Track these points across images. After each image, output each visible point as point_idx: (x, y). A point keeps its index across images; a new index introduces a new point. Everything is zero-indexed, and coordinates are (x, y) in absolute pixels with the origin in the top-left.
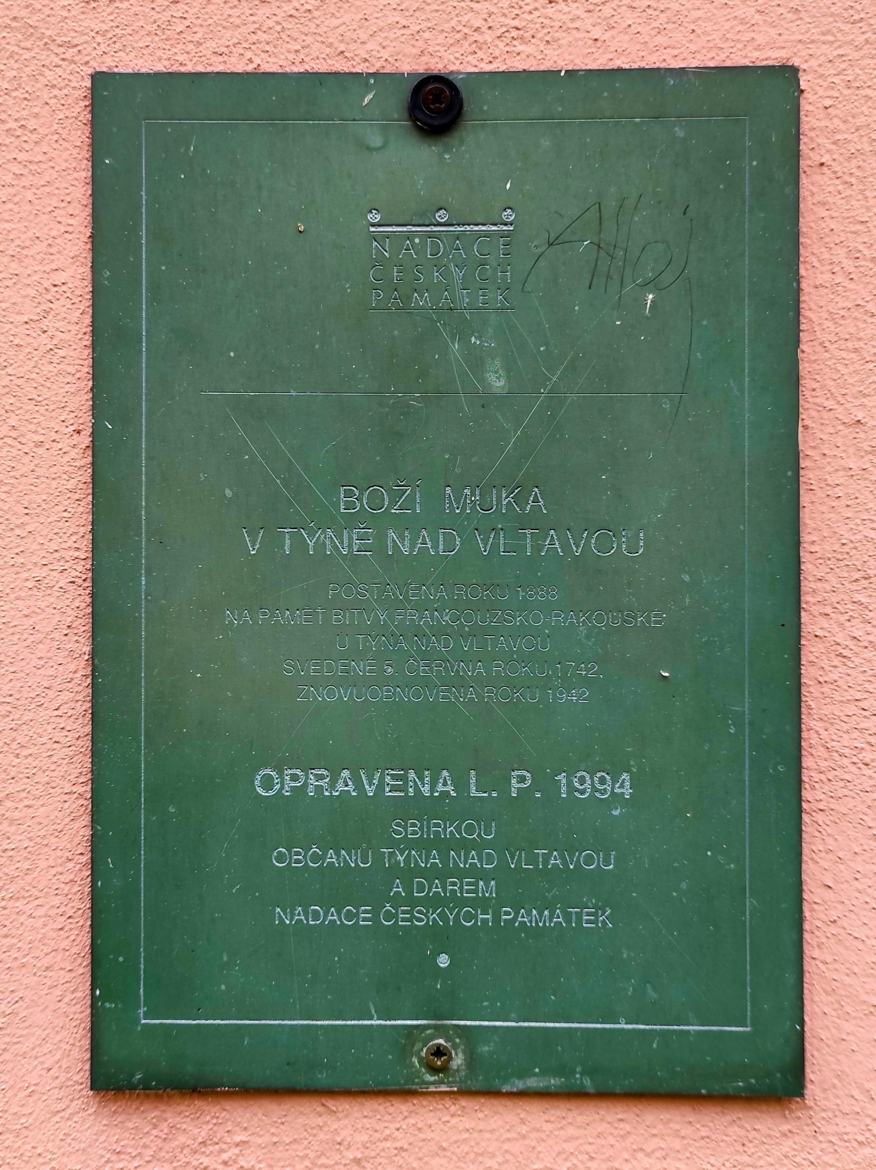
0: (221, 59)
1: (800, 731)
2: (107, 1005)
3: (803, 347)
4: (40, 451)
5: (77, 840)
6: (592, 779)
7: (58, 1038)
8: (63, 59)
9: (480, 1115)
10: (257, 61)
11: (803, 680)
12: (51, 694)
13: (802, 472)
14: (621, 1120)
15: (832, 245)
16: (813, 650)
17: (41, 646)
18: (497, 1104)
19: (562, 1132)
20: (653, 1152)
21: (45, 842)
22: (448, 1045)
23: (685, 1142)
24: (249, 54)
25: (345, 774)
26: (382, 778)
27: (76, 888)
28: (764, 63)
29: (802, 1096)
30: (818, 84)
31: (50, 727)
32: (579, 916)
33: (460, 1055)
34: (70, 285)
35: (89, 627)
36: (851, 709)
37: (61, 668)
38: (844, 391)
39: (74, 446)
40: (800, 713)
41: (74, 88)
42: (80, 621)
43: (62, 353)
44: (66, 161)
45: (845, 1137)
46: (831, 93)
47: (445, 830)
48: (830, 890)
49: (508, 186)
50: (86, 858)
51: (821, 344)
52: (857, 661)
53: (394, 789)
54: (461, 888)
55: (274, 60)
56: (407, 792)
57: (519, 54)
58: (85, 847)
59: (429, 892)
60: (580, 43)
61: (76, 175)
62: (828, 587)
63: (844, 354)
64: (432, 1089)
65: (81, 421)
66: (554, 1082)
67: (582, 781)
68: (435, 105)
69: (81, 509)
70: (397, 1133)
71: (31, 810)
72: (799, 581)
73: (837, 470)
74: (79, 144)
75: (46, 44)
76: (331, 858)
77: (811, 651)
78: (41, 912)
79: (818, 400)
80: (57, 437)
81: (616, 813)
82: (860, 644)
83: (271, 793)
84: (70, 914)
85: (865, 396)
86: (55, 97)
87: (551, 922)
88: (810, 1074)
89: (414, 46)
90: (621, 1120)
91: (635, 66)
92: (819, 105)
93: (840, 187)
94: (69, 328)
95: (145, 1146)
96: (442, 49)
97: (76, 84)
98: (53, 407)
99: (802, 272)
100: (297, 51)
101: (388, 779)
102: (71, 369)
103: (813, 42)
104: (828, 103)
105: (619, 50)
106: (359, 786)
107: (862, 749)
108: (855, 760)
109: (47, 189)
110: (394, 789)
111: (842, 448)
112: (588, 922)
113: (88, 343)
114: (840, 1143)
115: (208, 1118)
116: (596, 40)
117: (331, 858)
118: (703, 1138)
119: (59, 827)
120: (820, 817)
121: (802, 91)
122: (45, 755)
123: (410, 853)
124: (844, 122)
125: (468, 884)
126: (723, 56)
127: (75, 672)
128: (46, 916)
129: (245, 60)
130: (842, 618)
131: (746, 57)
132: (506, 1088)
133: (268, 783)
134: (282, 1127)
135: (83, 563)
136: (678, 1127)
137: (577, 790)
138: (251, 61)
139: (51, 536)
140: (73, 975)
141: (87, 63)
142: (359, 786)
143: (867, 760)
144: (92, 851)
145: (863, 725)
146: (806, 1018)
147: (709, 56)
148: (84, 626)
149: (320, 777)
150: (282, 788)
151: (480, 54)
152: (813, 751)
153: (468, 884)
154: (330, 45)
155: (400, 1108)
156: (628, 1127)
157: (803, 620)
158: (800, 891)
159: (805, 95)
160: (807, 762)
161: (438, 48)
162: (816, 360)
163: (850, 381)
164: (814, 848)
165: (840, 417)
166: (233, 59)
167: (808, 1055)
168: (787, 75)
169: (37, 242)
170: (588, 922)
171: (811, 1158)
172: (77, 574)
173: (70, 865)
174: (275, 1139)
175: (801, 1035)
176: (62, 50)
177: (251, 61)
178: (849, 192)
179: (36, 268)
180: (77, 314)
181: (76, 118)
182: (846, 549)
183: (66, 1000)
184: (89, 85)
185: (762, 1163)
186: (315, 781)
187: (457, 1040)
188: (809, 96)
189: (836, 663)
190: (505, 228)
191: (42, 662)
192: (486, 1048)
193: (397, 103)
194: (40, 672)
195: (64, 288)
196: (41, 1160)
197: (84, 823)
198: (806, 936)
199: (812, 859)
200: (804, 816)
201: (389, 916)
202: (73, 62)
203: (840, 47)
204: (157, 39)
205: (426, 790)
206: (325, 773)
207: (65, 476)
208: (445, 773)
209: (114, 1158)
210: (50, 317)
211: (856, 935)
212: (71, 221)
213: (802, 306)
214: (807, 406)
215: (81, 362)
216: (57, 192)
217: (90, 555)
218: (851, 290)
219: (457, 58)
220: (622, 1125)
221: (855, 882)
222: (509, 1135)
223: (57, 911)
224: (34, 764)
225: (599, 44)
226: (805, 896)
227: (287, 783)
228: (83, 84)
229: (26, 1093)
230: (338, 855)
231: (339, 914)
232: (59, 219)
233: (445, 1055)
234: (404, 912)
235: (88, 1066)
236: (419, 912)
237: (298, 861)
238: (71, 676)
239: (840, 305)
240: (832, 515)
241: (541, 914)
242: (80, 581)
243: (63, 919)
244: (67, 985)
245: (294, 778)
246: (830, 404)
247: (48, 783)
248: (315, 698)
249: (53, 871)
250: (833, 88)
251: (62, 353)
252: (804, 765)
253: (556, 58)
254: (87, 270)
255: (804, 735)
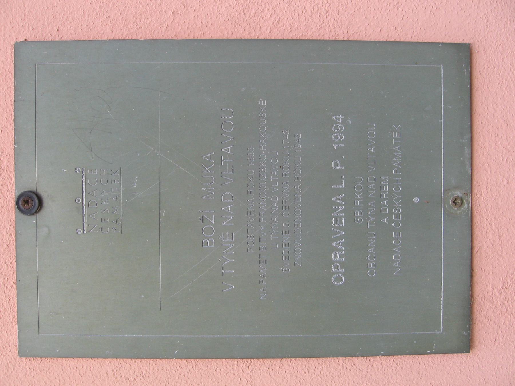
0: (11, 300)
1: (313, 40)
2: (434, 347)
3: (139, 38)
4: (189, 382)
5: (363, 362)
6: (335, 133)
7: (448, 367)
8: (14, 369)
9: (481, 183)
10: (12, 283)
11: (290, 38)
12: (299, 376)
13: (196, 38)
14: (482, 123)
15: (94, 25)
16: (276, 34)
17: (277, 380)
18: (475, 177)
19: (487, 148)
20: (494, 109)
21: (364, 376)
22: (452, 198)
23: (490, 95)
24: (9, 287)
25: (334, 244)
26: (335, 227)
27: (385, 362)
28: (13, 56)
29: (469, 44)
30: (23, 33)
31: (314, 376)
32: (396, 139)
33: (456, 192)
34: (114, 368)
35: (269, 360)
36: (302, 18)
37: (287, 372)
38: (159, 20)
39: (187, 367)
40: (305, 40)
41: (26, 365)
42: (266, 364)
43: (144, 372)
44: (58, 369)
45: (485, 27)
46: (27, 27)
47: (359, 199)
48: (383, 29)
49: (65, 170)
50: (372, 358)
51: (138, 30)
52: (281, 15)
53: (341, 222)
54: (385, 192)
55: (11, 276)
56: (342, 217)
57: (8, 166)
58: (367, 359)
59: (387, 206)
60: (3, 138)
61: (65, 365)
62: (248, 27)
63: (143, 20)
64: (470, 205)
65: (175, 364)
66: (467, 151)
67: (336, 137)
68: (30, 203)
69: (215, 364)
70: (489, 220)
71: (350, 383)
72: (245, 39)
73: (195, 23)
74: (51, 363)
75: (7, 377)
76: (372, 250)
77: (277, 35)
78: (394, 377)
79: (163, 31)
80: (182, 374)
81: (350, 122)
82: (273, 13)
83: (343, 278)
84: (395, 364)
85: (161, 11)
86: (30, 373)
87: (399, 152)
88: (460, 41)
89: (4, 213)
90: (482, 123)
91: (13, 113)
92: (32, 32)
93: (68, 22)
94: (133, 369)
95: (493, 329)
96: (6, 201)
97: (24, 365)
98: (169, 376)
99: (105, 38)
100: (7, 266)
101: (337, 225)
102: (152, 368)
103: (4, 35)
104: (31, 28)
105: (6, 121)
106: (340, 238)
107: (320, 13)
108: (325, 17)
109: (71, 377)
110: (341, 222)
111: (185, 20)
112: (398, 135)
113: (139, 360)
114: (488, 29)
115: (482, 302)
116: (1, 131)
117: (372, 250)
118: (488, 87)
119: (358, 370)
120: (351, 33)
121: (26, 40)
122: (326, 378)
123: (369, 215)
124: (39, 21)
125: (383, 189)
126: (10, 75)
127: (289, 365)
128: (396, 375)
129: (12, 289)
130: (262, 21)
131: (10, 65)
132: (470, 171)
133: (338, 279)
134: (486, 270)
135: (239, 363)
136: (484, 98)
137: (341, 139)
138: (12, 287)
139: (227, 377)
140: (421, 362)
141: (15, 359)
142: (340, 238)
143: (325, 12)
144: (368, 356)
145: (310, 13)
146: (437, 42)
147: (9, 81)
148: (269, 362)
149: (336, 256)
150: (340, 273)
151: (8, 183)
152: (321, 35)
153: (383, 189)
154: (4, 251)
155: (477, 219)
156: (485, 120)
157: (263, 38)
158: (383, 42)
159: (27, 38)
160: (326, 38)
161: (5, 202)
162: (145, 32)
163: (155, 17)
164: (364, 36)
165: (171, 21)
166: (11, 294)
167: (452, 42)
168: (19, 48)
169: (95, 382)
170: (398, 135)
171: (494, 42)
172: (244, 365)
173: (374, 365)
174: (491, 273)
175: (443, 44)
176: (10, 370)
177: (12, 287)
178: (71, 19)
179: (107, 383)
180: (127, 365)
181: (39, 364)
182: (230, 19)
183: (432, 365)
184: (24, 358)
185: (497, 63)
186: (337, 257)
187: (450, 194)
188: (28, 37)
189: (282, 24)
190: (84, 172)
191: (285, 380)
192: (453, 181)
193: (32, 220)
194: (289, 381)
195: (115, 371)
196: (498, 373)
197: (356, 360)
198: (402, 40)
199: (369, 37)
200: (350, 39)
201: (397, 224)
202: (15, 365)
203: (7, 24)
204: (3, 328)
205: (341, 208)
206: (334, 253)
207: (200, 371)
208: (334, 199)
209: (497, 341)
210: (128, 377)
211: (401, 19)
212: (85, 367)
213: (120, 39)
214: (166, 36)
215: (148, 364)
216: (72, 373)
217: (236, 360)
218: (114, 17)
219: (9, 194)
220: (484, 122)
221: (379, 18)
222: (489, 171)
223: (394, 370)
224: (330, 382)
225: (3, 130)
226: (385, 40)
227: (337, 270)
228: (24, 361)
229: (470, 380)
230: (370, 247)
231: (396, 247)
232: (84, 372)
233: (456, 199)
234: (395, 217)
235: (460, 354)
236: (395, 211)
237: (373, 265)
238: (291, 367)
239: (120, 21)
240: (215, 25)
241: (395, 156)
242: (248, 364)
243: (398, 368)
244: (426, 364)
245: (336, 267)
246: (165, 25)
247: (339, 376)
248: (300, 258)
249: (377, 372)
250: (25, 26)
251: (144, 372)
252: (328, 39)
253: (10, 149)
254: (107, 361)
255: (314, 38)
